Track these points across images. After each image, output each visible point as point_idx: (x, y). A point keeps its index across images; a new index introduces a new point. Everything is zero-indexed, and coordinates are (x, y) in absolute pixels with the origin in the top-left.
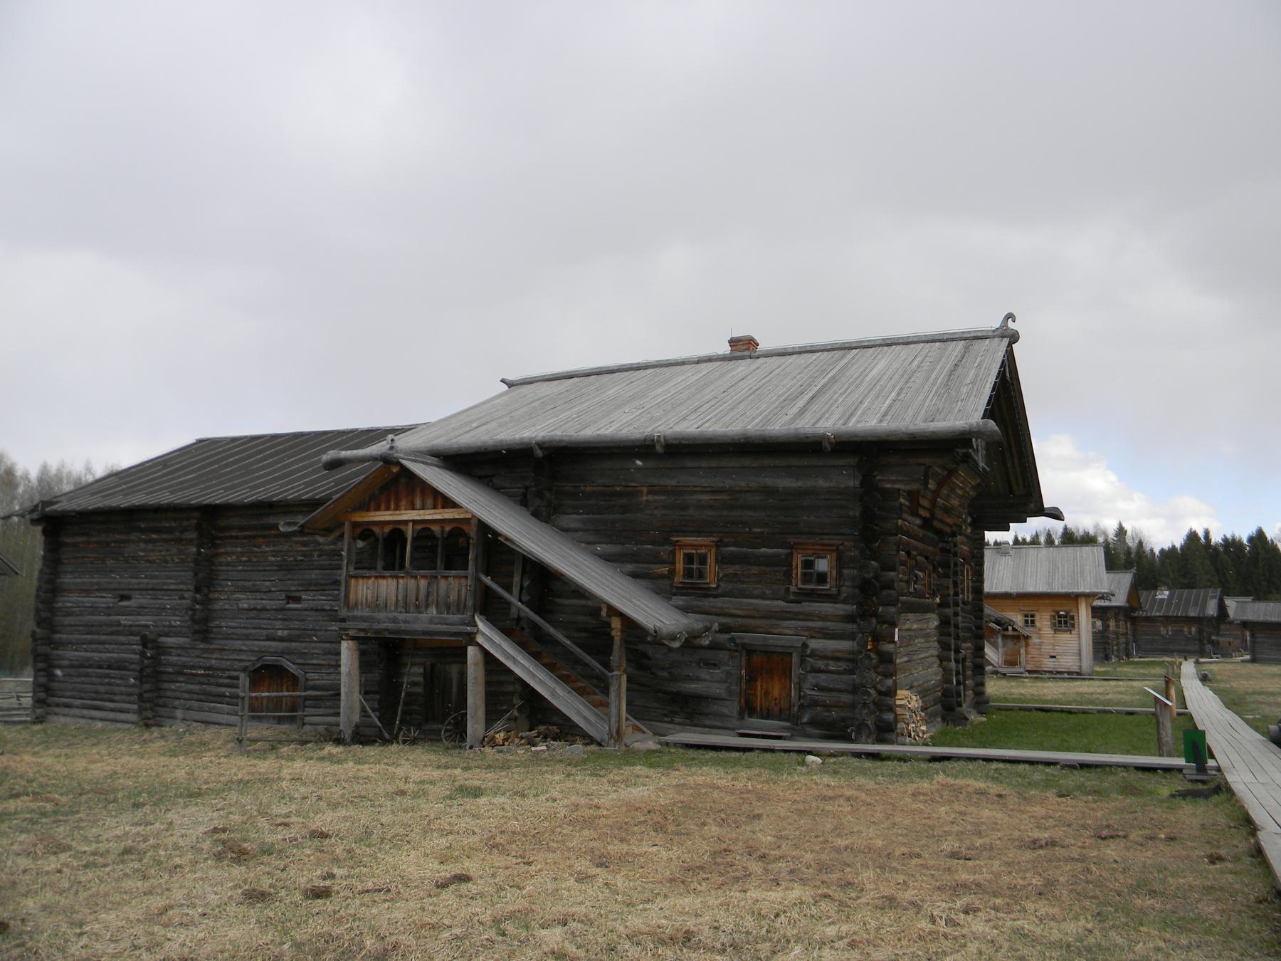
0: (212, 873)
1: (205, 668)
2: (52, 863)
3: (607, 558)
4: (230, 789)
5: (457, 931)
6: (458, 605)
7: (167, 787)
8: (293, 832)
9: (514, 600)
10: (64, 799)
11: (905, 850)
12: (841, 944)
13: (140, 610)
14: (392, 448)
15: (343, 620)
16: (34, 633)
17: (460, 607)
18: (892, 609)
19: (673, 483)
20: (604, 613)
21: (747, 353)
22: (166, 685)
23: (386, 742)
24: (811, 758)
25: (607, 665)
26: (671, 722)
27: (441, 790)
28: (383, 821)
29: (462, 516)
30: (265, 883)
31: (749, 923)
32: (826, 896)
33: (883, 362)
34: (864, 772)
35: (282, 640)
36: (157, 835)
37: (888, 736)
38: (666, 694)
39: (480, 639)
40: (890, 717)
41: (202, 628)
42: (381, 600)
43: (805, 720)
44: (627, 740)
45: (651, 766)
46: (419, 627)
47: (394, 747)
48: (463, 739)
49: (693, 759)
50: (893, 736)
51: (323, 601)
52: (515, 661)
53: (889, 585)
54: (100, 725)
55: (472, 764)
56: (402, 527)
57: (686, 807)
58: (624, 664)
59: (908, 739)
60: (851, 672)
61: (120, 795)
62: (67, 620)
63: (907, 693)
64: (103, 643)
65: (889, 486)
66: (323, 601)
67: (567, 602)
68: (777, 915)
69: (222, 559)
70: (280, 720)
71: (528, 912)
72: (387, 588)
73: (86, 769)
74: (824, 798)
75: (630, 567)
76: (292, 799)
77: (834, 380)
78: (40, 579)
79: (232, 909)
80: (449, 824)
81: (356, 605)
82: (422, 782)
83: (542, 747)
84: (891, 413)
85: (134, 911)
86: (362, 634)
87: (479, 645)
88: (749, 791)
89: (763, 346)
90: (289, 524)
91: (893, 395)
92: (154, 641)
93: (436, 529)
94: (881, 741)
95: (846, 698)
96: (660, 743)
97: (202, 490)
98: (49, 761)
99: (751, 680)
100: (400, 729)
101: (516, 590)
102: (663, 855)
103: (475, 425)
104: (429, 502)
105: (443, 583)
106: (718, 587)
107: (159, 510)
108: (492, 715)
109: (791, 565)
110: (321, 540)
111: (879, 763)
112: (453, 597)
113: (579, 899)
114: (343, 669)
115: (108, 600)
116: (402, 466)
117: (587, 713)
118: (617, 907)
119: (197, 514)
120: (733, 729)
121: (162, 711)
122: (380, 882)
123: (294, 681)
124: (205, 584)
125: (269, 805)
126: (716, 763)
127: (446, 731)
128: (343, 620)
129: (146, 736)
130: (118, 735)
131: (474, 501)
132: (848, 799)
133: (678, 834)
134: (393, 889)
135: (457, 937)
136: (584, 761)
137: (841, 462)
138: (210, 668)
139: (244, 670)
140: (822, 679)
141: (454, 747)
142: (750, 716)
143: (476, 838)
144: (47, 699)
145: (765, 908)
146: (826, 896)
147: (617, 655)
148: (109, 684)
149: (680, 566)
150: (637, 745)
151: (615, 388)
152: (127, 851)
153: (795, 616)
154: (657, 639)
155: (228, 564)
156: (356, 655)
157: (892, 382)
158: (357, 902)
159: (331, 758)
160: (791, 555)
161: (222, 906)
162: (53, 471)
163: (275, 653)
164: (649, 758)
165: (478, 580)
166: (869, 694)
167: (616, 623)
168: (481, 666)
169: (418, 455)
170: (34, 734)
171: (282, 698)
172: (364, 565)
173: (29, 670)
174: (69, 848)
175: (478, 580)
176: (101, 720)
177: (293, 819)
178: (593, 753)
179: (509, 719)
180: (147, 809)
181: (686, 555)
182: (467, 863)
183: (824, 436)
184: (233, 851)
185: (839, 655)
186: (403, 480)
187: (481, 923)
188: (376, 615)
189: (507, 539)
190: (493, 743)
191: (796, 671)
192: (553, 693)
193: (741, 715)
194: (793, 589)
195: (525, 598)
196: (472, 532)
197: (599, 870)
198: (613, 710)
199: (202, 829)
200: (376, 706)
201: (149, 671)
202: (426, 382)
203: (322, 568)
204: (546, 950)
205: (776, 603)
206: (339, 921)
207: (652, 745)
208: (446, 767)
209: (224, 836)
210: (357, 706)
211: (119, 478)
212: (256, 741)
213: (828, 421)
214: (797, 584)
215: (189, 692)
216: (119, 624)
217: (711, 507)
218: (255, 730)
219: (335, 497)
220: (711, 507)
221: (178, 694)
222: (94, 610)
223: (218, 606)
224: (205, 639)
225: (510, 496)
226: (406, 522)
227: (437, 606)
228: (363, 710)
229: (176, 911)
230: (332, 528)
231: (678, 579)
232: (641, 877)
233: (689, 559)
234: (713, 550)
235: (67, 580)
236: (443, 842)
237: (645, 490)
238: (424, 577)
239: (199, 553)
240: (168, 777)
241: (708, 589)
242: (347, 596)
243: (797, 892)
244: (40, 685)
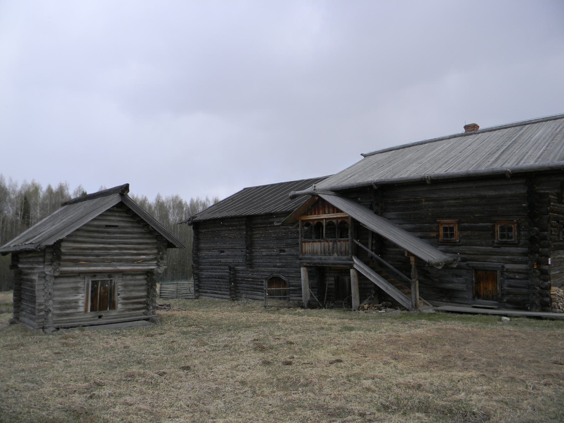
0: (253, 354)
1: (252, 278)
2: (202, 349)
3: (408, 230)
4: (261, 325)
5: (333, 379)
6: (345, 252)
7: (239, 323)
8: (281, 342)
9: (369, 251)
10: (206, 327)
11: (531, 359)
12: (482, 393)
13: (228, 256)
14: (315, 190)
15: (301, 259)
16: (193, 266)
17: (346, 253)
18: (547, 249)
19: (436, 196)
20: (406, 255)
21: (473, 132)
22: (238, 285)
23: (321, 308)
24: (504, 318)
25: (409, 277)
26: (442, 301)
27: (338, 328)
28: (314, 339)
29: (345, 216)
30: (270, 359)
31: (447, 383)
32: (483, 375)
33: (542, 131)
34: (530, 325)
35: (279, 267)
36: (235, 341)
37: (547, 308)
38: (436, 289)
39: (355, 266)
40: (548, 300)
41: (250, 263)
42: (315, 251)
43: (505, 301)
44: (420, 308)
45: (430, 320)
46: (330, 262)
47: (324, 310)
48: (351, 307)
49: (449, 317)
50: (550, 309)
51: (293, 251)
52: (370, 275)
53: (545, 238)
54: (217, 299)
55: (353, 317)
56: (321, 221)
57: (438, 338)
58: (417, 276)
59: (558, 310)
60: (527, 279)
61: (223, 326)
62: (203, 261)
63: (556, 288)
64: (216, 269)
65: (542, 191)
66: (293, 251)
67: (392, 249)
68: (459, 381)
69: (255, 236)
70: (280, 299)
71: (361, 374)
72: (317, 246)
73: (212, 316)
74: (504, 336)
75: (419, 234)
76: (282, 329)
77: (515, 142)
78: (193, 246)
79: (258, 367)
80: (338, 341)
81: (305, 253)
82: (331, 324)
83: (383, 311)
84: (542, 157)
85: (228, 365)
86: (308, 265)
87: (354, 268)
88: (469, 332)
89: (481, 127)
90: (278, 222)
91: (544, 147)
92: (233, 268)
93: (334, 221)
94: (543, 310)
95: (525, 291)
96: (435, 310)
97: (246, 209)
98: (201, 313)
99: (478, 282)
100: (326, 303)
101: (370, 246)
102: (422, 356)
103: (349, 176)
104: (331, 210)
105: (338, 243)
106: (460, 241)
107: (232, 218)
108: (362, 298)
109: (494, 230)
110: (290, 227)
111: (539, 321)
112: (343, 249)
113: (380, 370)
114: (302, 279)
115: (216, 253)
116: (320, 197)
117: (402, 297)
118: (396, 374)
119: (245, 219)
120: (470, 304)
121: (238, 294)
122: (309, 361)
123: (284, 284)
124: (250, 246)
125: (273, 332)
126: (459, 319)
127: (345, 303)
128: (301, 259)
129: (233, 304)
130: (224, 304)
131: (348, 209)
132: (515, 337)
133: (431, 348)
134: (314, 363)
135: (333, 381)
136: (400, 317)
137: (517, 182)
138: (254, 278)
139: (266, 279)
140: (512, 282)
141: (348, 310)
142: (478, 299)
143: (347, 347)
144: (199, 290)
145: (455, 378)
146: (483, 375)
147: (414, 272)
148: (219, 284)
149: (441, 233)
150: (425, 311)
151: (410, 154)
152: (226, 346)
153: (497, 254)
154: (429, 264)
155: (257, 238)
156: (307, 273)
157: (545, 140)
158: (300, 367)
159: (299, 314)
160: (494, 226)
161: (255, 366)
162: (195, 201)
163: (277, 272)
164: (429, 317)
165: (353, 242)
166: (536, 289)
167: (412, 259)
168: (356, 277)
169: (326, 191)
170: (196, 303)
171: (280, 290)
172: (308, 237)
173: (192, 279)
174: (208, 344)
175: (353, 242)
176: (218, 298)
177: (282, 337)
178: (404, 314)
179: (370, 299)
180: (232, 332)
181: (444, 227)
182: (342, 356)
183: (507, 171)
184: (260, 347)
185: (521, 271)
186: (320, 202)
187: (342, 377)
188: (314, 257)
189: (363, 225)
190: (363, 309)
191: (499, 278)
192: (387, 288)
193: (474, 298)
194: (496, 241)
195: (374, 248)
196: (349, 221)
197: (393, 361)
198: (413, 296)
199: (250, 339)
200: (316, 293)
201: (232, 279)
202: (328, 157)
203: (292, 238)
204: (364, 386)
205: (488, 248)
206: (294, 373)
207: (431, 311)
208: (343, 319)
209: (257, 342)
210: (309, 293)
211: (218, 205)
212: (271, 307)
213: (509, 163)
214: (498, 239)
215: (247, 287)
216: (221, 262)
217: (454, 206)
218: (270, 303)
219: (295, 210)
220: (454, 206)
221: (243, 288)
222: (212, 257)
223: (255, 254)
224: (251, 267)
225: (365, 206)
226: (322, 219)
227: (337, 253)
228: (311, 295)
229: (241, 366)
230: (294, 223)
231: (441, 238)
232: (410, 364)
233: (445, 229)
234: (457, 225)
235: (202, 245)
236: (335, 347)
237: (424, 200)
238: (331, 241)
239: (247, 234)
240: (240, 320)
241: (455, 242)
242: (302, 250)
243: (474, 373)
244: (196, 285)
